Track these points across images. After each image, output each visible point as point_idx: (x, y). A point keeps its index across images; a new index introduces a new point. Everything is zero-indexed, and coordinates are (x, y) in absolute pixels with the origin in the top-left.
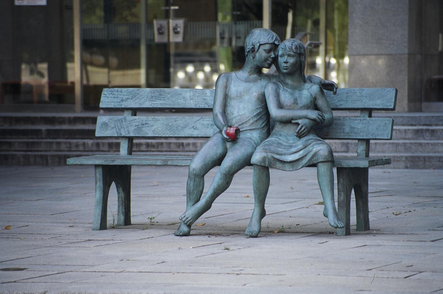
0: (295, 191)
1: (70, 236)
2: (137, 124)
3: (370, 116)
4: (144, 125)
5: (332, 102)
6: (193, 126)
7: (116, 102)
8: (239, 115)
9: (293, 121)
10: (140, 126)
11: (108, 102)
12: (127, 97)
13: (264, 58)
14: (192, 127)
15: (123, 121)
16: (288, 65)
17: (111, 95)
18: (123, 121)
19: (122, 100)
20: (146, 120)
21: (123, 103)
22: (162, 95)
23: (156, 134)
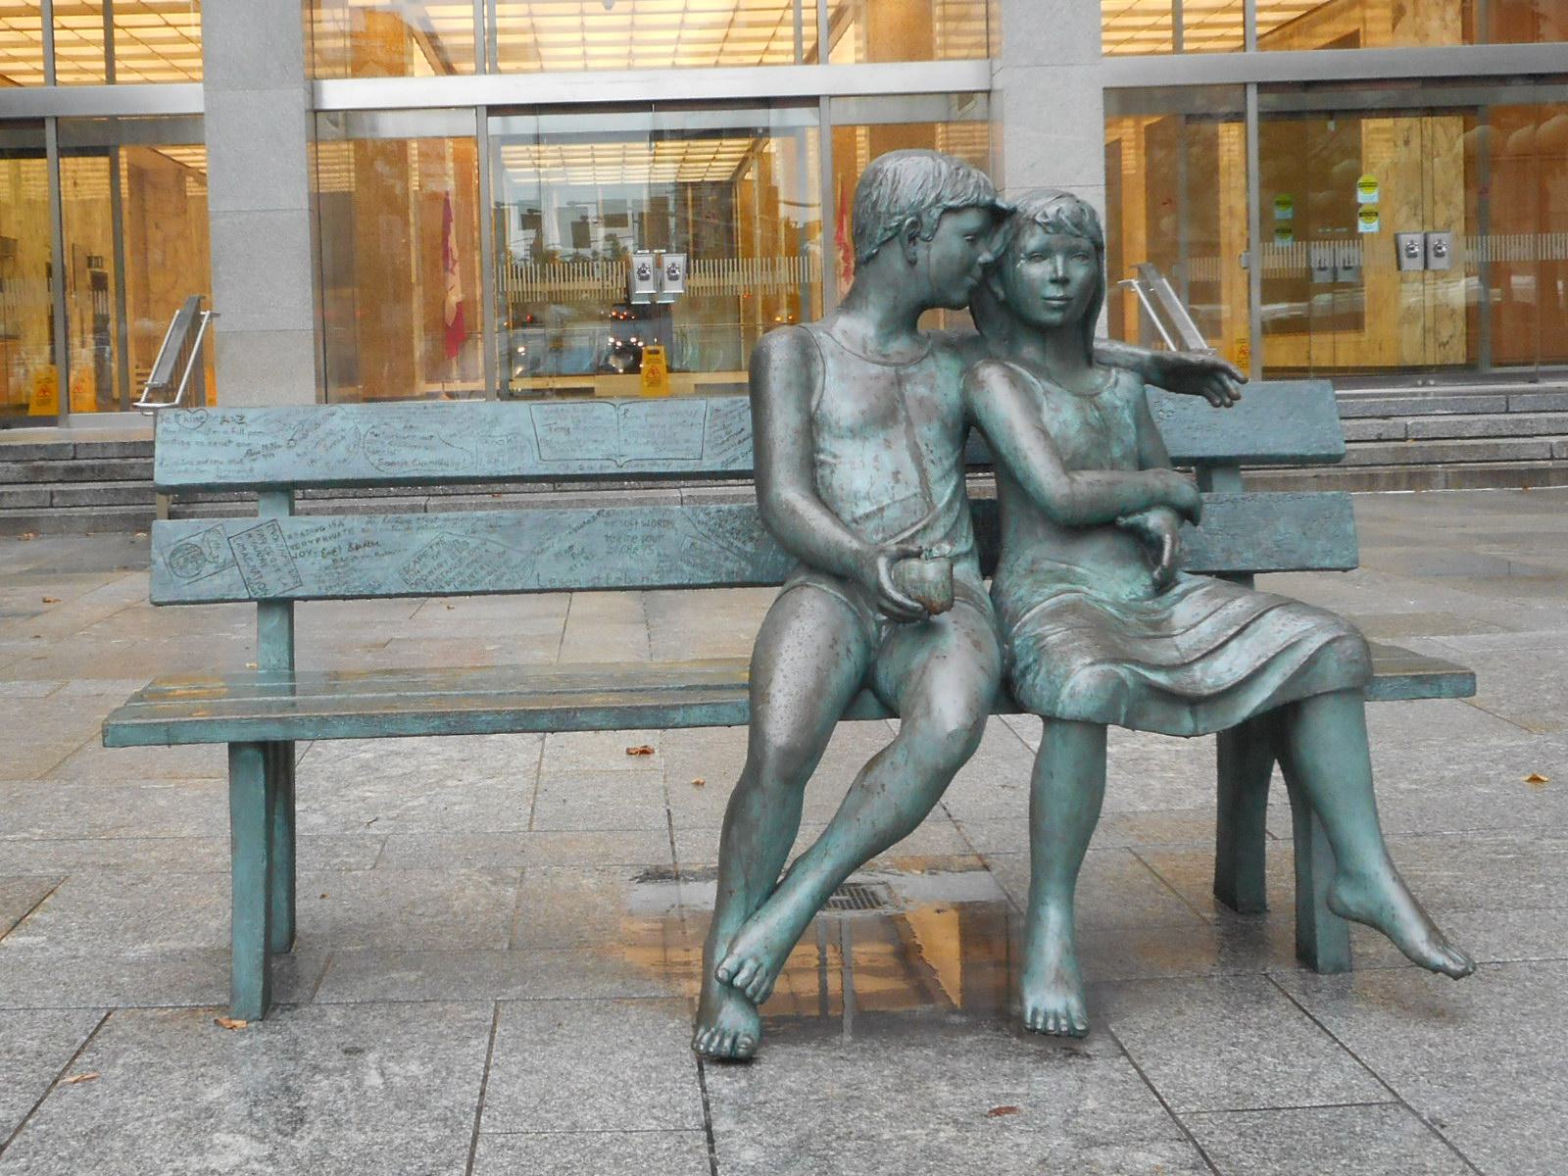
0: (86, 1042)
1: (672, 810)
2: (330, 545)
3: (218, 315)
4: (361, 552)
5: (939, 374)
6: (571, 547)
7: (225, 460)
8: (894, 502)
9: (1122, 521)
10: (344, 554)
11: (191, 463)
12: (268, 440)
13: (939, 262)
14: (566, 552)
15: (267, 533)
16: (1072, 289)
17: (200, 437)
18: (267, 533)
19: (250, 453)
20: (363, 530)
21: (256, 465)
22: (416, 428)
23: (416, 584)
